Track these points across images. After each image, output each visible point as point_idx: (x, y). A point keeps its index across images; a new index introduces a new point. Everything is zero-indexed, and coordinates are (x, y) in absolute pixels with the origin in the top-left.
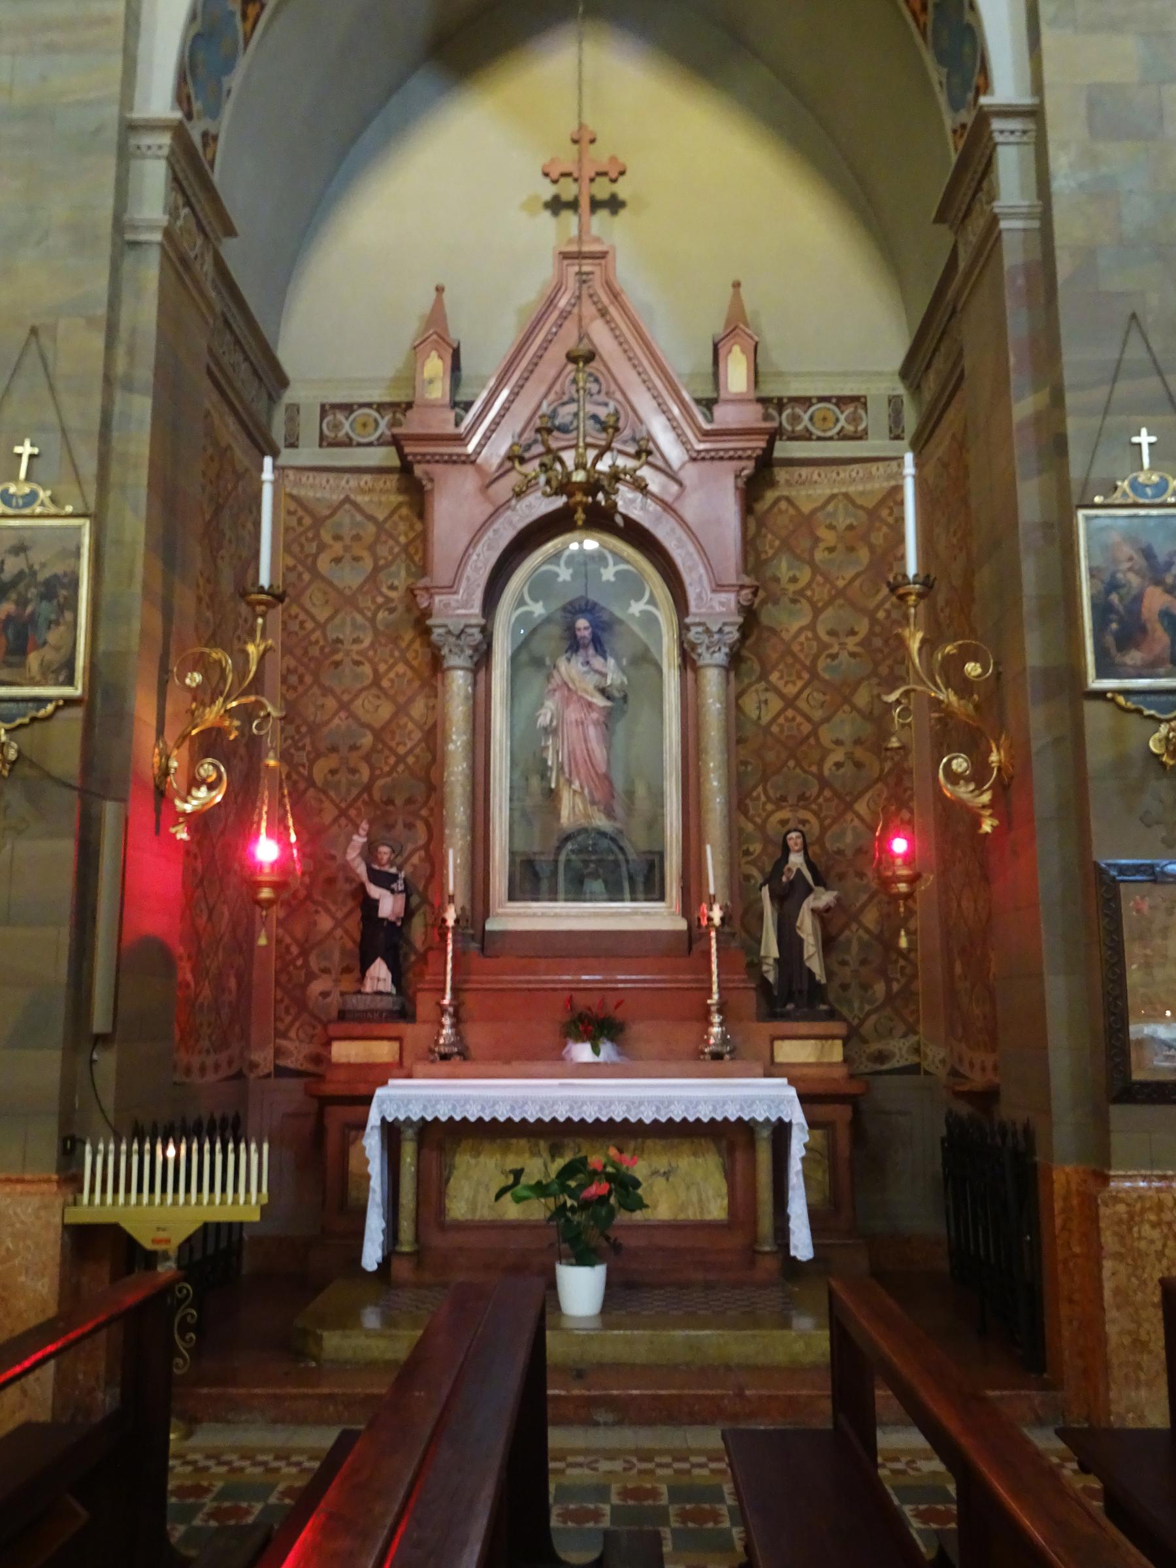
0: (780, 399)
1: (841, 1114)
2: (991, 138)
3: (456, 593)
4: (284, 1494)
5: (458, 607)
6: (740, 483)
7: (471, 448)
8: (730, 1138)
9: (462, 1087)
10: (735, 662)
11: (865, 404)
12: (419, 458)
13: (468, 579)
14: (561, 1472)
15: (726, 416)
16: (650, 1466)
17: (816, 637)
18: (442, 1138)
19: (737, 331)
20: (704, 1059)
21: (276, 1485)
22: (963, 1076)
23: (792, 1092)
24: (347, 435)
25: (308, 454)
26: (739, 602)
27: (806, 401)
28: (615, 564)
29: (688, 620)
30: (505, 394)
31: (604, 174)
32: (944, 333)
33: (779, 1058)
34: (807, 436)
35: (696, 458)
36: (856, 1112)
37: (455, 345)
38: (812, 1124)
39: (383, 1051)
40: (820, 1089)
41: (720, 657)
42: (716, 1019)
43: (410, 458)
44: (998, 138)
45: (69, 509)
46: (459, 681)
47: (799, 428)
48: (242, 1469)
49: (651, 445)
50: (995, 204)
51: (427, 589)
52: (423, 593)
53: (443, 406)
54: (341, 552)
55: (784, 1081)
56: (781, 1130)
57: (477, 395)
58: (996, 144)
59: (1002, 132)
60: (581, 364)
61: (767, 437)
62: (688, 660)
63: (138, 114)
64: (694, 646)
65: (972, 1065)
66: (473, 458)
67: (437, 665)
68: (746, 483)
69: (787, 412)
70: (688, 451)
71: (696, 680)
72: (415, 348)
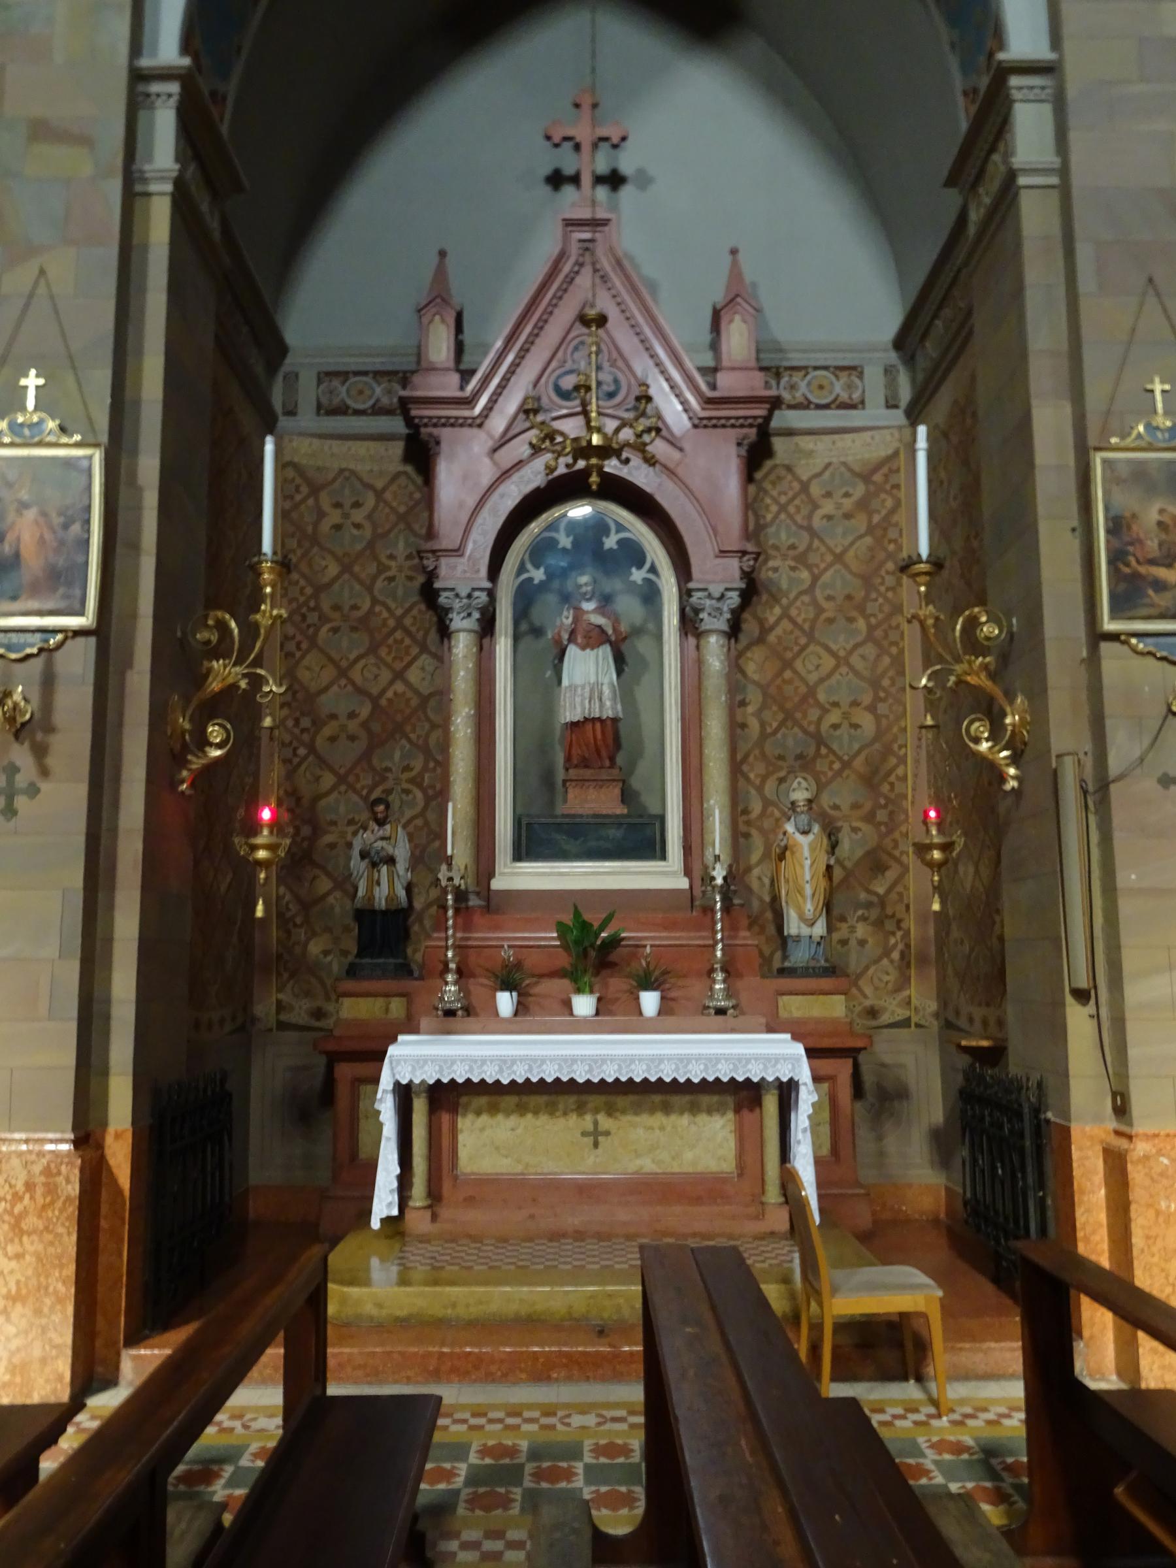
0: (778, 368)
1: (843, 1069)
2: (1008, 96)
3: (462, 555)
4: (256, 1456)
5: (463, 574)
6: (743, 452)
7: (478, 410)
8: (743, 1095)
9: (480, 1043)
10: (734, 630)
11: (862, 373)
12: (426, 420)
13: (475, 542)
14: (446, 1428)
15: (728, 383)
16: (545, 1421)
17: (815, 602)
18: (447, 1097)
19: (739, 300)
20: (709, 1015)
21: (248, 1445)
22: (960, 1030)
23: (799, 1049)
24: (343, 401)
25: (307, 419)
26: (741, 568)
27: (804, 369)
28: (528, 571)
29: (691, 585)
30: (510, 358)
31: (606, 139)
32: (944, 299)
33: (783, 1014)
34: (805, 405)
35: (699, 424)
36: (856, 1067)
37: (458, 308)
38: (817, 1079)
39: (397, 1007)
40: (826, 1043)
41: (722, 624)
42: (719, 976)
43: (417, 421)
44: (1016, 95)
45: (77, 438)
46: (462, 645)
47: (798, 395)
48: (232, 1430)
49: (660, 425)
50: (1013, 160)
51: (434, 552)
52: (430, 555)
53: (447, 369)
54: (353, 511)
55: (788, 1036)
56: (787, 1091)
57: (480, 363)
58: (1014, 101)
59: (1020, 88)
60: (594, 329)
61: (768, 406)
62: (689, 623)
63: (145, 62)
64: (697, 611)
65: (971, 1020)
66: (478, 421)
67: (445, 632)
68: (748, 451)
69: (785, 380)
70: (690, 418)
71: (698, 647)
72: (419, 311)
